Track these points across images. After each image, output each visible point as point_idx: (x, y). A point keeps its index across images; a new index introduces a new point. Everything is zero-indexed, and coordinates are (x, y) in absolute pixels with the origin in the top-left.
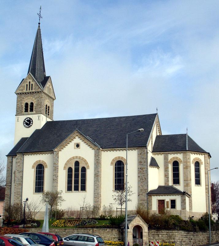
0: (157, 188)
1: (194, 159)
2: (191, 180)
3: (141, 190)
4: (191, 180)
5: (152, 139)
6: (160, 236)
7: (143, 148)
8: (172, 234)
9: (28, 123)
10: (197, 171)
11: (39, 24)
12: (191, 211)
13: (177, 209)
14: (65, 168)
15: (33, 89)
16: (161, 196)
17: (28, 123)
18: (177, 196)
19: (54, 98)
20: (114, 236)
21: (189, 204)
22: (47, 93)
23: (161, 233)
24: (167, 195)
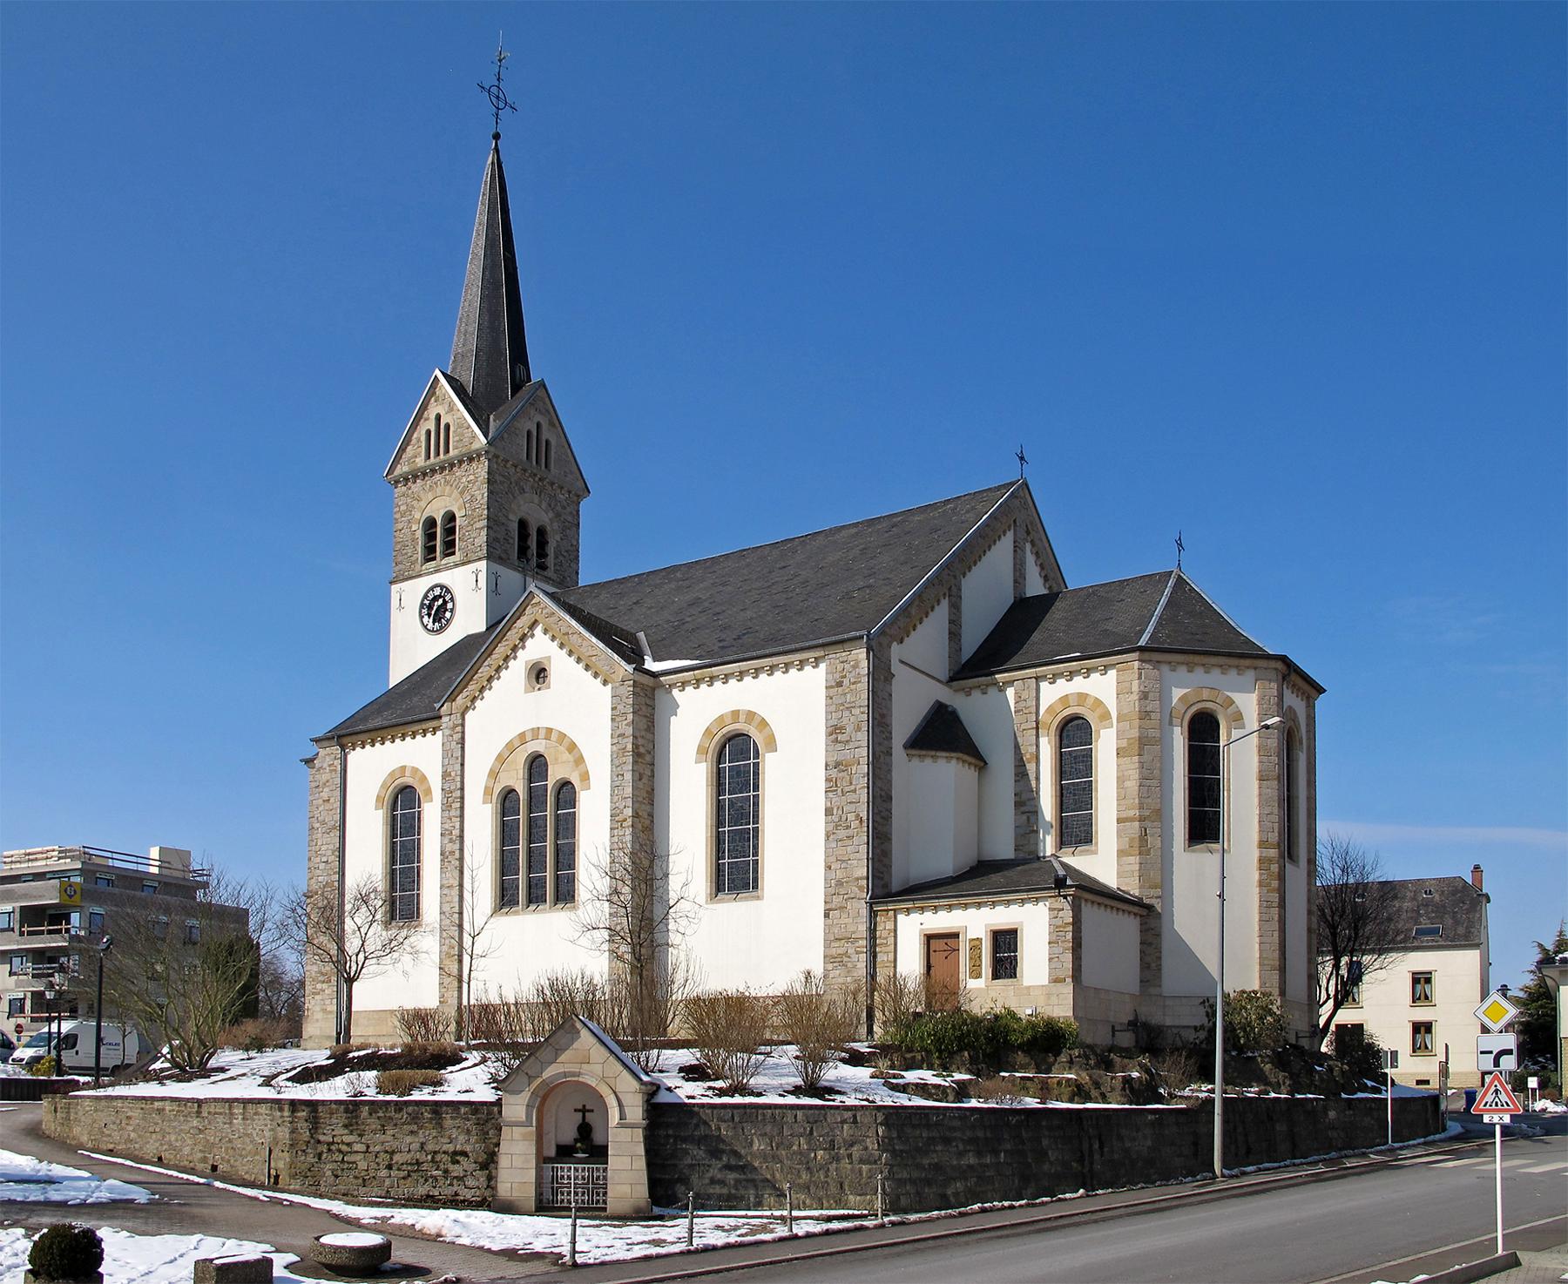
3: (840, 883)
9: (438, 609)
11: (497, 137)
12: (1153, 991)
13: (1026, 982)
14: (488, 791)
20: (450, 1148)
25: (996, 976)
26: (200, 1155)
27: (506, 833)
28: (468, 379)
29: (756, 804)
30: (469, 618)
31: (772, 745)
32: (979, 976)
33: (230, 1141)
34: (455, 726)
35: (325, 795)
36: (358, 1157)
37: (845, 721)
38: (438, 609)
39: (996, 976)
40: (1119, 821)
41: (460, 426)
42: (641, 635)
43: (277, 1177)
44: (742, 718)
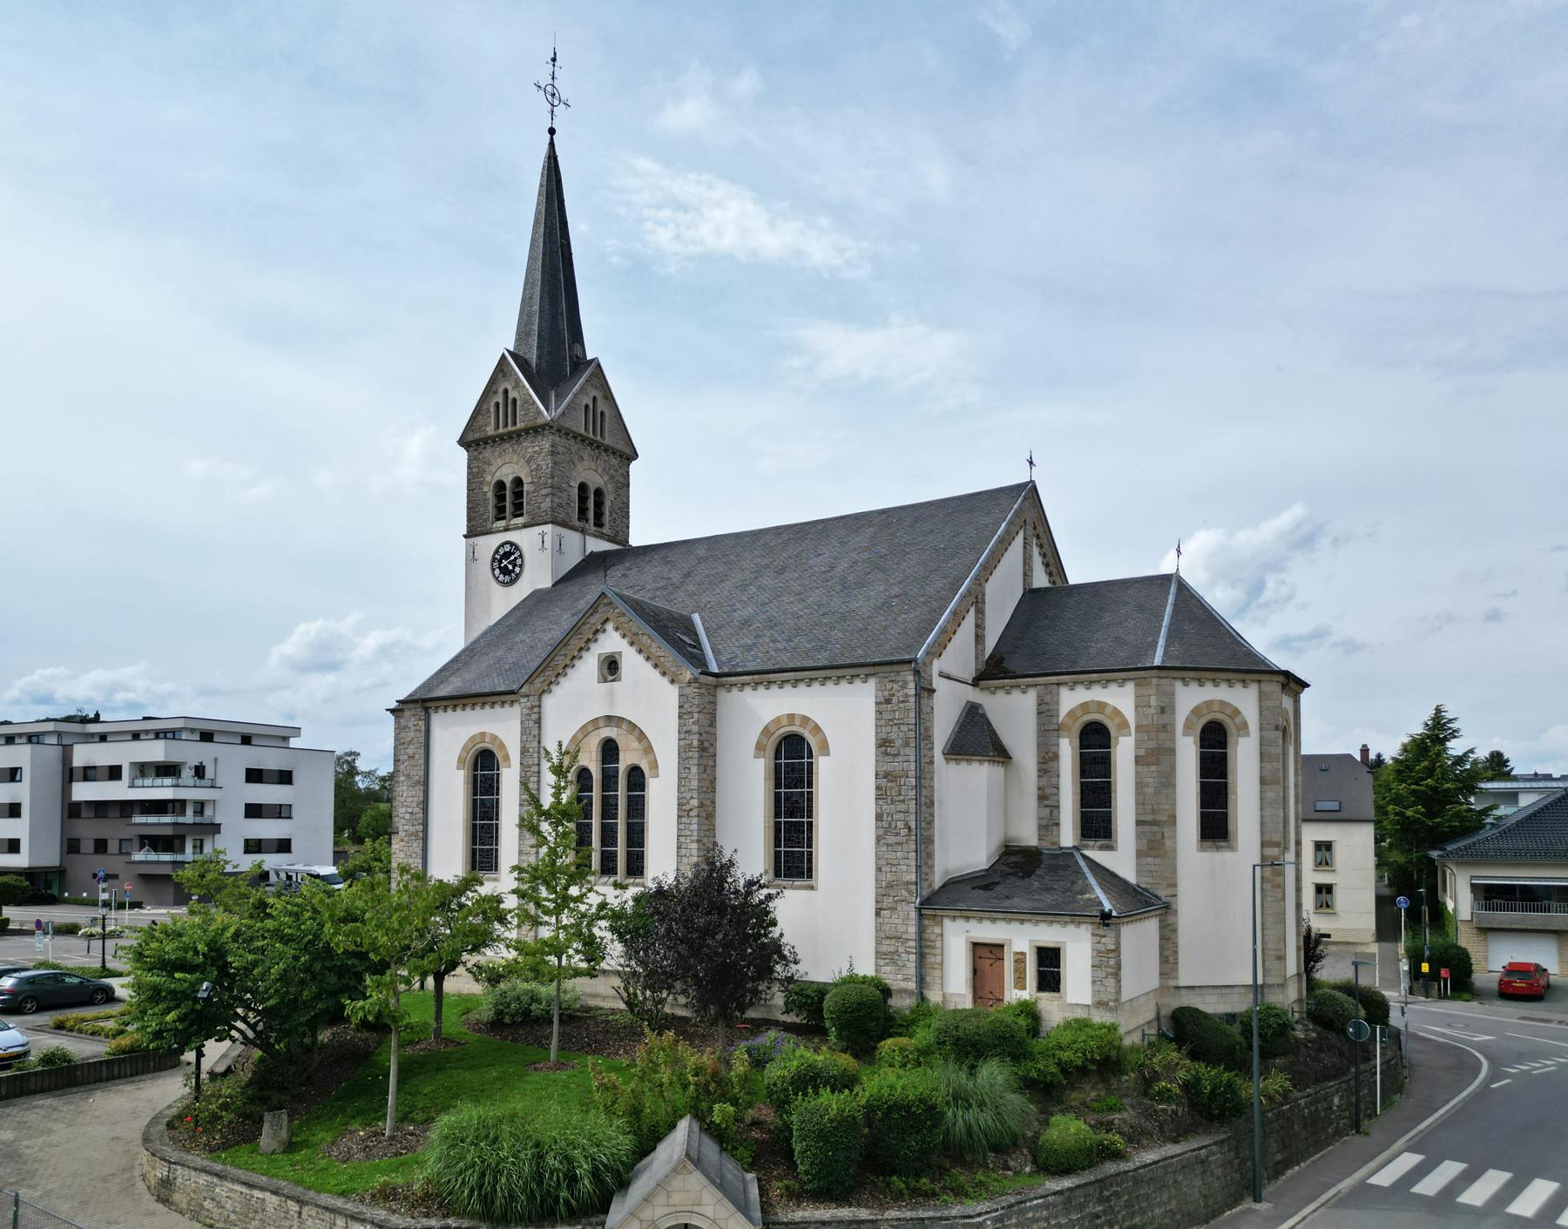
2: (1173, 819)
5: (980, 613)
7: (896, 668)
9: (507, 565)
10: (1215, 768)
11: (552, 131)
16: (986, 924)
17: (507, 565)
18: (1071, 928)
19: (627, 450)
21: (1162, 948)
22: (582, 431)
28: (533, 357)
29: (810, 800)
31: (825, 750)
32: (1024, 988)
34: (532, 707)
40: (1139, 823)
41: (526, 401)
42: (696, 617)
44: (797, 722)
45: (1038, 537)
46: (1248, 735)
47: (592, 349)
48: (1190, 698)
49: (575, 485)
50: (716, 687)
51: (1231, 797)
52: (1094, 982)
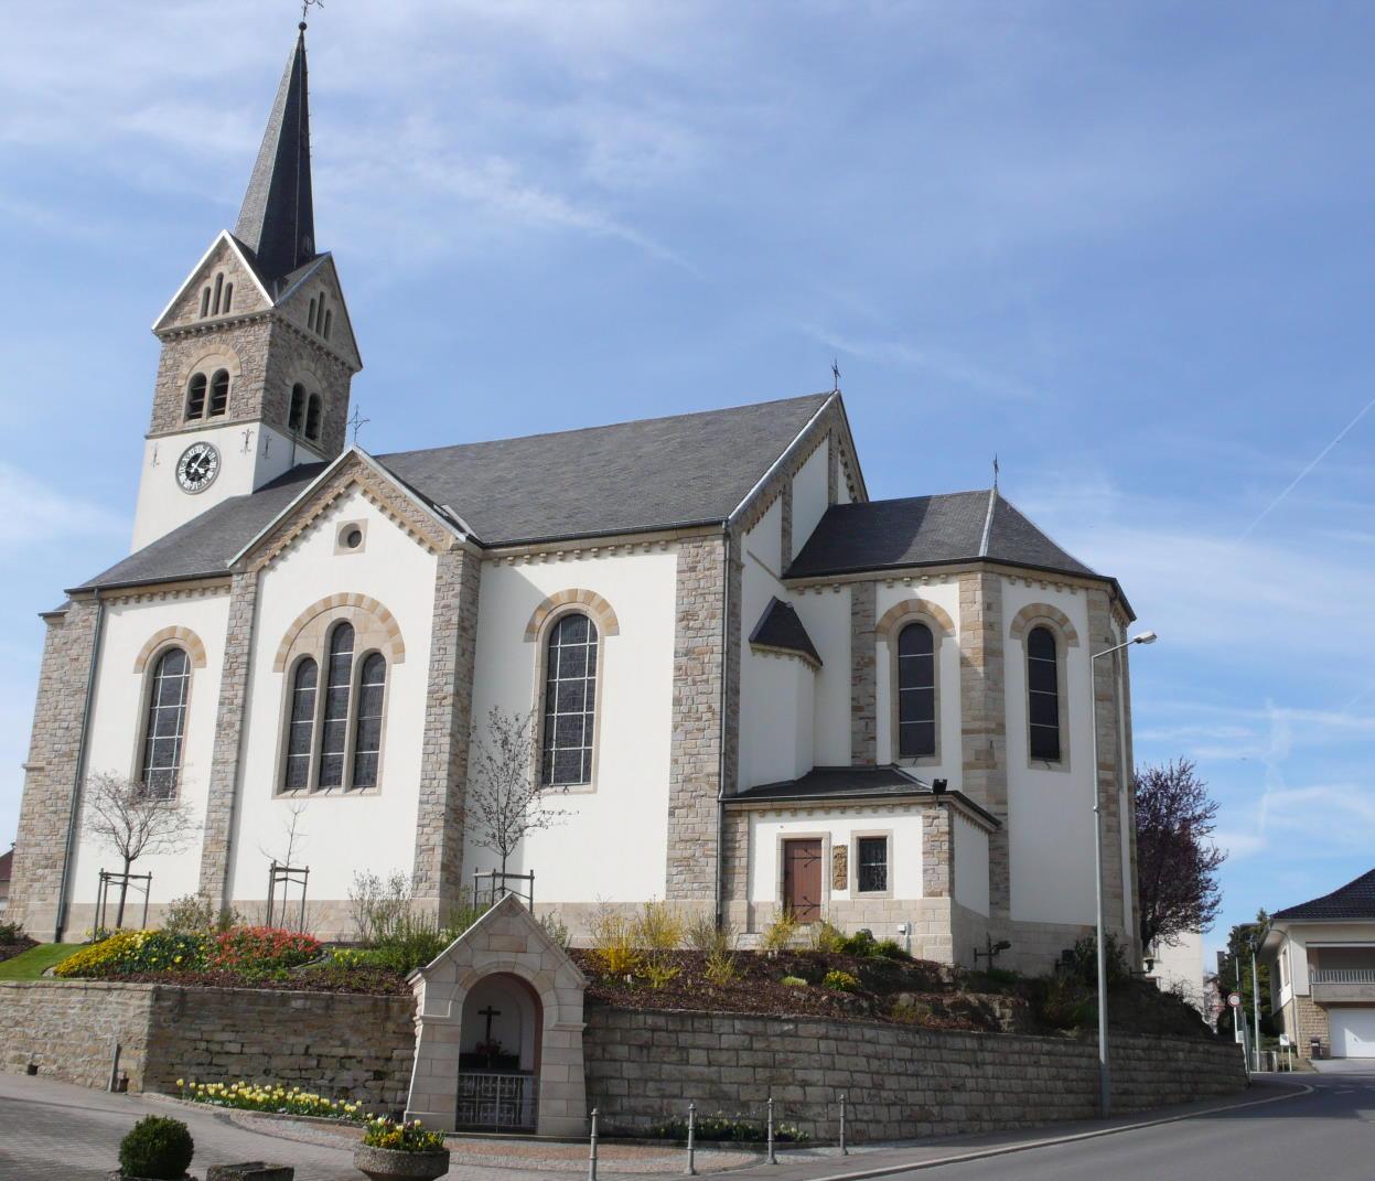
0: (795, 779)
1: (1023, 613)
4: (1004, 734)
5: (787, 505)
6: (698, 1056)
8: (789, 1044)
9: (197, 469)
11: (303, 26)
12: (1002, 914)
14: (281, 659)
15: (232, 307)
19: (353, 363)
20: (341, 1052)
23: (702, 1039)
24: (822, 808)
25: (862, 888)
26: (13, 1053)
27: (296, 706)
28: (254, 242)
29: (591, 690)
30: (237, 475)
31: (613, 627)
32: (844, 887)
33: (60, 1036)
35: (73, 653)
36: (232, 1059)
37: (698, 606)
38: (197, 469)
39: (862, 888)
41: (244, 287)
43: (126, 1081)
45: (843, 454)
46: (1077, 645)
47: (323, 241)
48: (1020, 596)
49: (290, 384)
50: (481, 561)
51: (1061, 712)
52: (925, 871)
